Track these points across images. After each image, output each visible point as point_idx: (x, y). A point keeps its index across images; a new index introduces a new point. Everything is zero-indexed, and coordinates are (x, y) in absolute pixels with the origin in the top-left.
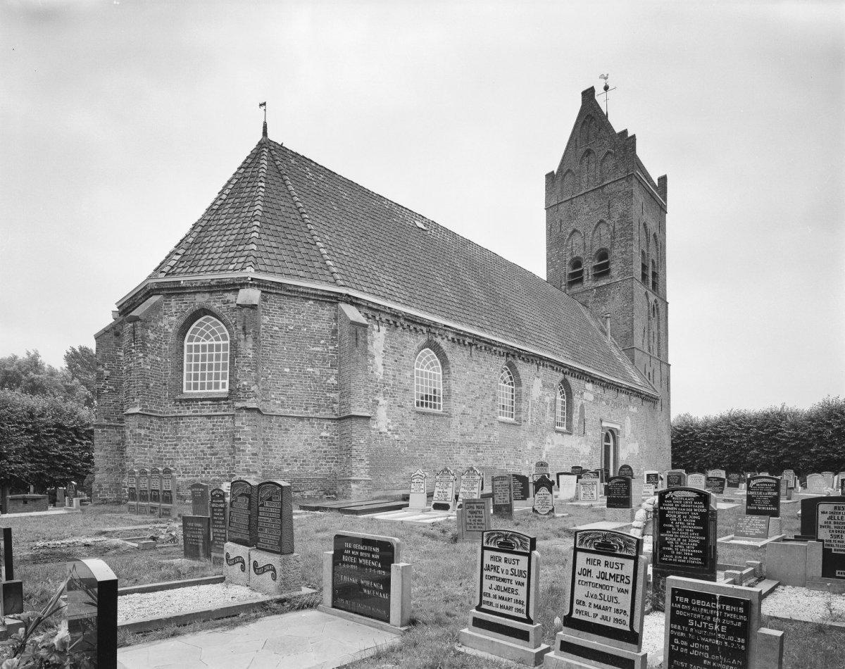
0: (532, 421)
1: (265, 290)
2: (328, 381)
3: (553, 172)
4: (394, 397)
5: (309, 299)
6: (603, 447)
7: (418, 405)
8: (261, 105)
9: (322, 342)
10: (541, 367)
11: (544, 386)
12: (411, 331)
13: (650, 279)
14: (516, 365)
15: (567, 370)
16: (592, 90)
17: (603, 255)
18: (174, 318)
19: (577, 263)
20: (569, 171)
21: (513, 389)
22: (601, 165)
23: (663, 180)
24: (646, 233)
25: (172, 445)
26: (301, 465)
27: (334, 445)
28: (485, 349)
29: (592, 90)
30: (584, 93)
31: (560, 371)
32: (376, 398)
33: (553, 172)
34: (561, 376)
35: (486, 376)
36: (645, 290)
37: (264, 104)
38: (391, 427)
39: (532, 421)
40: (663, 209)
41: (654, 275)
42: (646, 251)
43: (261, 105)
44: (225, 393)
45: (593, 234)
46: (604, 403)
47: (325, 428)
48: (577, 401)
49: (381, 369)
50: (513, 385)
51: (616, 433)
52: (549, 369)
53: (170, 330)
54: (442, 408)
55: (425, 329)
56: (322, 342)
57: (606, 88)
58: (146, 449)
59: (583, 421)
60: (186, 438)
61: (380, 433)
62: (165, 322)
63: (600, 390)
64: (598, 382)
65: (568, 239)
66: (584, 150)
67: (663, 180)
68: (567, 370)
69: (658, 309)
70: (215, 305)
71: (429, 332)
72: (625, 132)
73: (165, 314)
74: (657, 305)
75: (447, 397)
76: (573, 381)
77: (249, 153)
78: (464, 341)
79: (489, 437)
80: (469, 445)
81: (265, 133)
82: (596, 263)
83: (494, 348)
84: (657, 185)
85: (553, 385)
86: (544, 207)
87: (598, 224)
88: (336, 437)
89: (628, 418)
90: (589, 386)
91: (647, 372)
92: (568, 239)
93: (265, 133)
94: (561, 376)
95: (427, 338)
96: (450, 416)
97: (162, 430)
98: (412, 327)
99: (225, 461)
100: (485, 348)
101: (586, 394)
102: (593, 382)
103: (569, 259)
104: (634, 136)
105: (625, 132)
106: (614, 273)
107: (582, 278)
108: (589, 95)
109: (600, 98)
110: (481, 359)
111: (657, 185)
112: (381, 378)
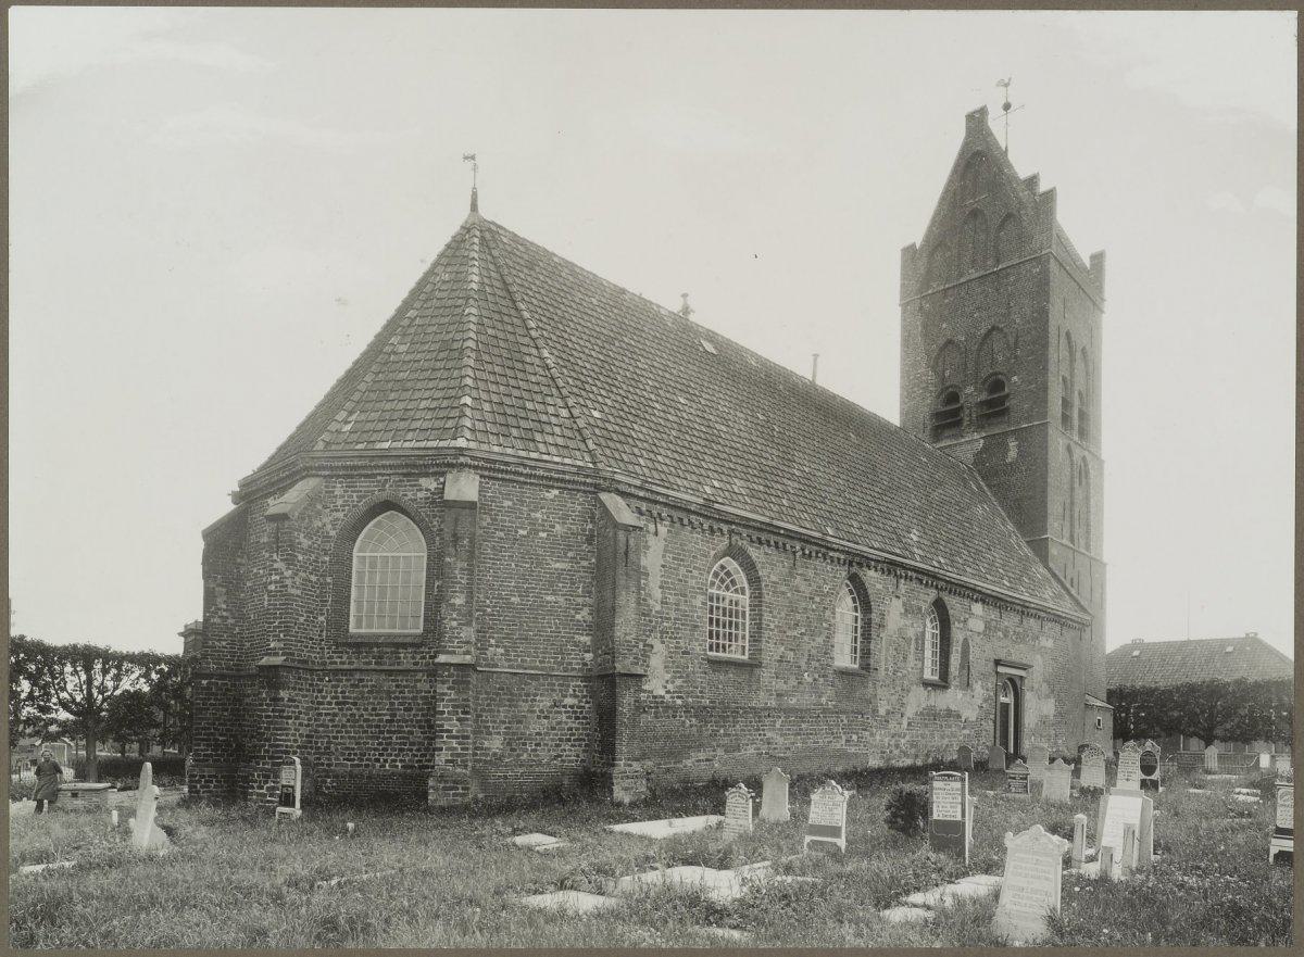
0: (887, 669)
1: (486, 473)
2: (578, 617)
3: (914, 245)
4: (676, 638)
5: (553, 487)
6: (998, 706)
7: (711, 649)
8: (466, 158)
9: (570, 554)
10: (903, 581)
11: (906, 610)
12: (703, 531)
13: (1076, 422)
14: (864, 578)
15: (941, 584)
16: (983, 111)
18: (340, 515)
21: (856, 617)
23: (1098, 259)
24: (1070, 347)
25: (329, 714)
26: (532, 750)
27: (584, 718)
28: (817, 557)
29: (983, 111)
30: (970, 117)
31: (932, 585)
32: (649, 641)
33: (914, 245)
34: (933, 594)
35: (817, 599)
36: (1067, 441)
37: (473, 158)
38: (670, 687)
39: (887, 669)
41: (1083, 416)
42: (1069, 378)
43: (466, 158)
44: (416, 636)
46: (1000, 634)
47: (571, 691)
48: (958, 635)
49: (658, 594)
50: (857, 611)
51: (1018, 682)
52: (914, 584)
53: (333, 533)
54: (747, 653)
55: (725, 528)
56: (570, 554)
57: (1007, 107)
58: (290, 721)
59: (966, 665)
60: (352, 703)
61: (655, 697)
62: (326, 520)
63: (994, 614)
64: (992, 599)
67: (1098, 259)
68: (941, 584)
69: (1087, 473)
70: (406, 495)
71: (731, 532)
72: (1032, 181)
73: (325, 507)
74: (1086, 465)
75: (596, 485)
76: (954, 603)
77: (448, 240)
78: (784, 545)
79: (820, 697)
80: (788, 711)
81: (474, 207)
82: (984, 396)
83: (831, 554)
84: (1088, 266)
85: (920, 609)
86: (898, 302)
87: (990, 332)
88: (587, 705)
89: (1038, 656)
90: (978, 608)
91: (1069, 578)
93: (474, 207)
94: (933, 594)
95: (727, 542)
96: (759, 665)
97: (314, 691)
98: (706, 526)
99: (412, 744)
100: (817, 553)
101: (973, 619)
102: (983, 602)
104: (1050, 196)
105: (1032, 181)
107: (962, 419)
108: (977, 122)
109: (996, 124)
110: (811, 573)
111: (1088, 266)
112: (658, 608)
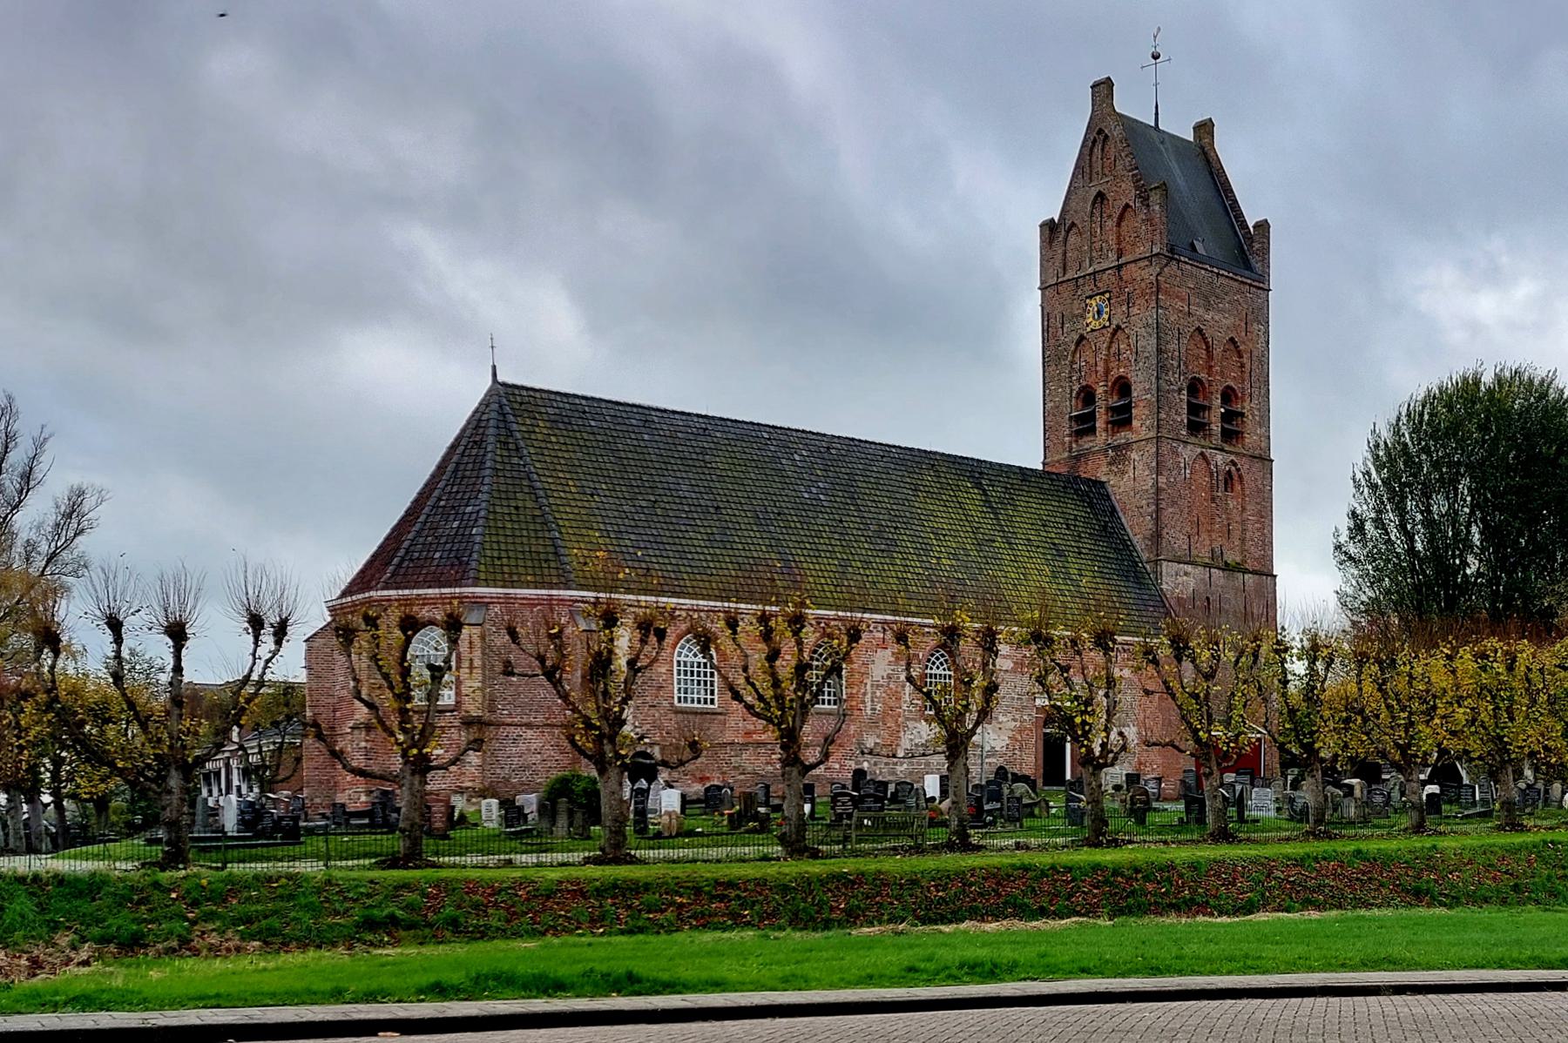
17: (1123, 387)
19: (1087, 396)
20: (1073, 224)
22: (1119, 225)
23: (1263, 226)
40: (1260, 283)
45: (1109, 348)
65: (1074, 352)
66: (1094, 192)
67: (1263, 226)
69: (1240, 477)
81: (494, 375)
92: (1074, 352)
93: (494, 375)
103: (1076, 387)
106: (1135, 423)
